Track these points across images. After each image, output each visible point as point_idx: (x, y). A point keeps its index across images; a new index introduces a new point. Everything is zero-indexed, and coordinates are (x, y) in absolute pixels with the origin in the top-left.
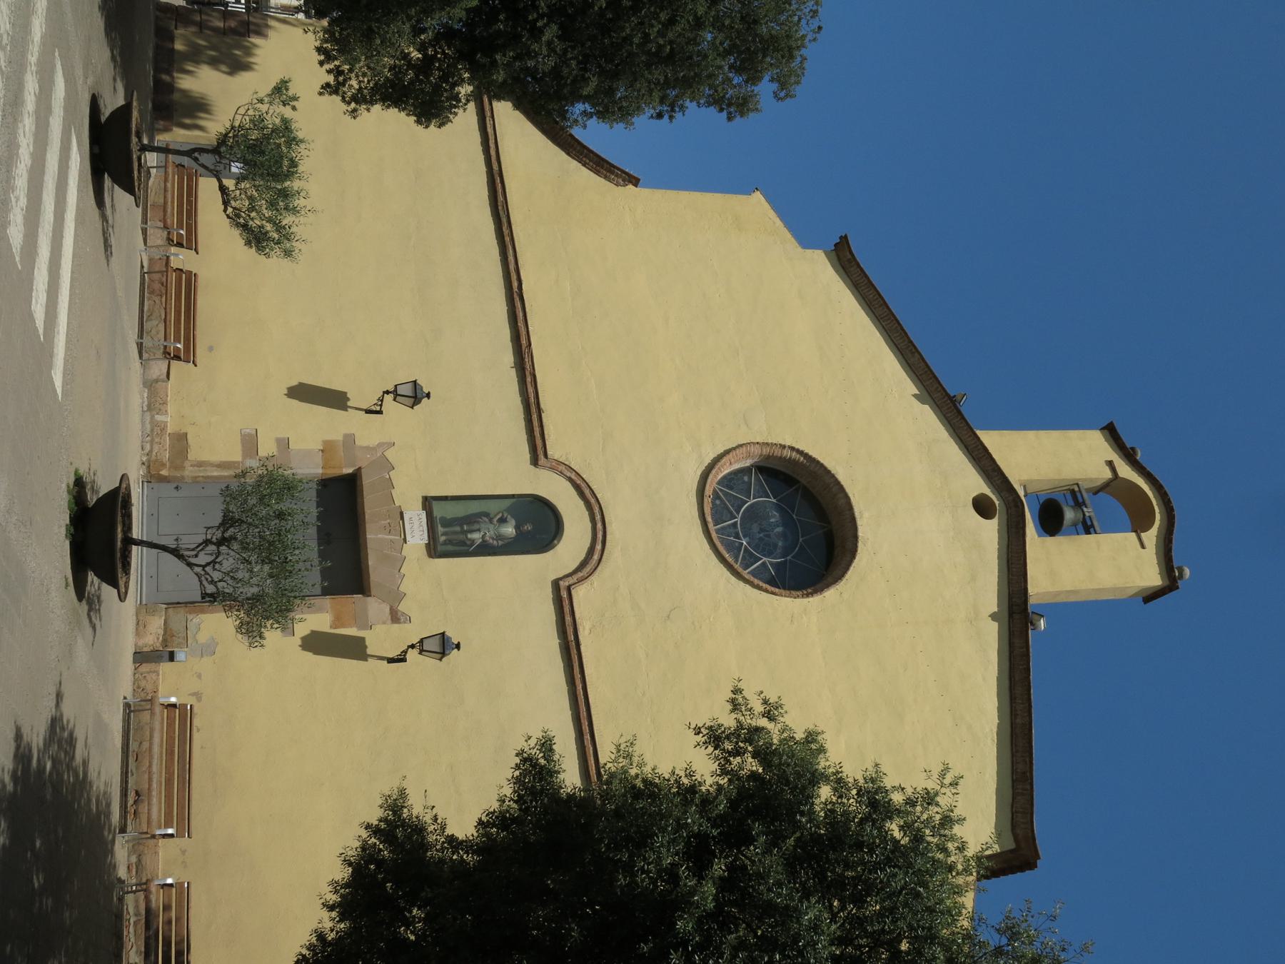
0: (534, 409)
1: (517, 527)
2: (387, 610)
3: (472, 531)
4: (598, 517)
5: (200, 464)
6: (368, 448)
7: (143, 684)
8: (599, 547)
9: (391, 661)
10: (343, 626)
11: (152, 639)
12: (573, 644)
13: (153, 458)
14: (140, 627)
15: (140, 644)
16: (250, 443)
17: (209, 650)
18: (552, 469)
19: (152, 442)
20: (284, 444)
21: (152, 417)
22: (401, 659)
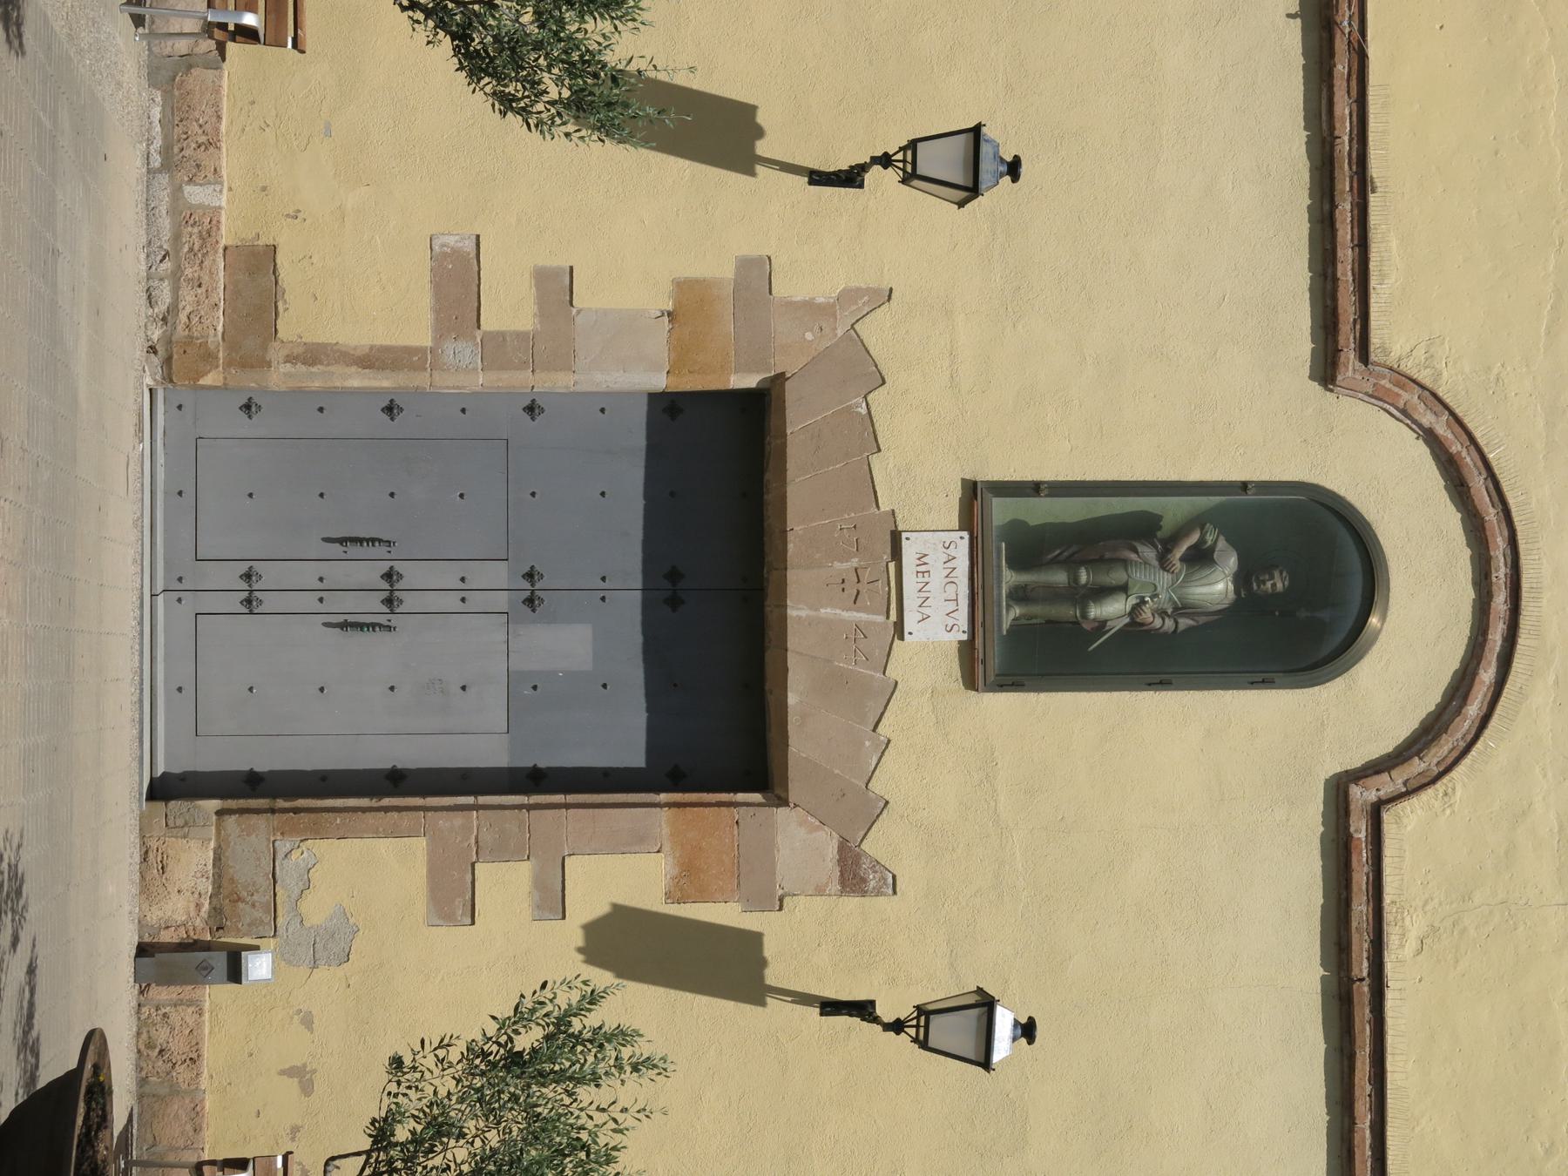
0: (1344, 183)
1: (1242, 579)
2: (832, 851)
3: (1102, 592)
4: (1500, 573)
5: (312, 355)
6: (809, 306)
7: (162, 1035)
8: (1487, 675)
9: (818, 178)
10: (703, 896)
11: (182, 908)
12: (1363, 990)
13: (181, 332)
14: (152, 868)
15: (154, 916)
16: (457, 281)
17: (330, 947)
18: (1377, 396)
19: (176, 277)
20: (556, 289)
21: (177, 191)
22: (851, 178)
